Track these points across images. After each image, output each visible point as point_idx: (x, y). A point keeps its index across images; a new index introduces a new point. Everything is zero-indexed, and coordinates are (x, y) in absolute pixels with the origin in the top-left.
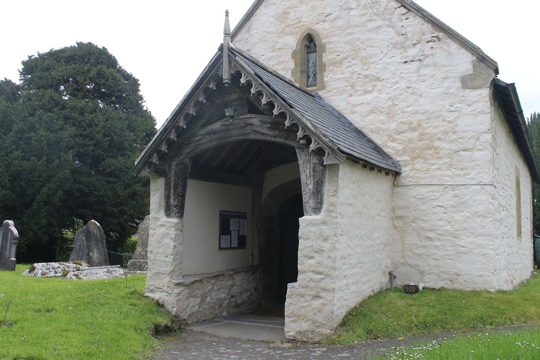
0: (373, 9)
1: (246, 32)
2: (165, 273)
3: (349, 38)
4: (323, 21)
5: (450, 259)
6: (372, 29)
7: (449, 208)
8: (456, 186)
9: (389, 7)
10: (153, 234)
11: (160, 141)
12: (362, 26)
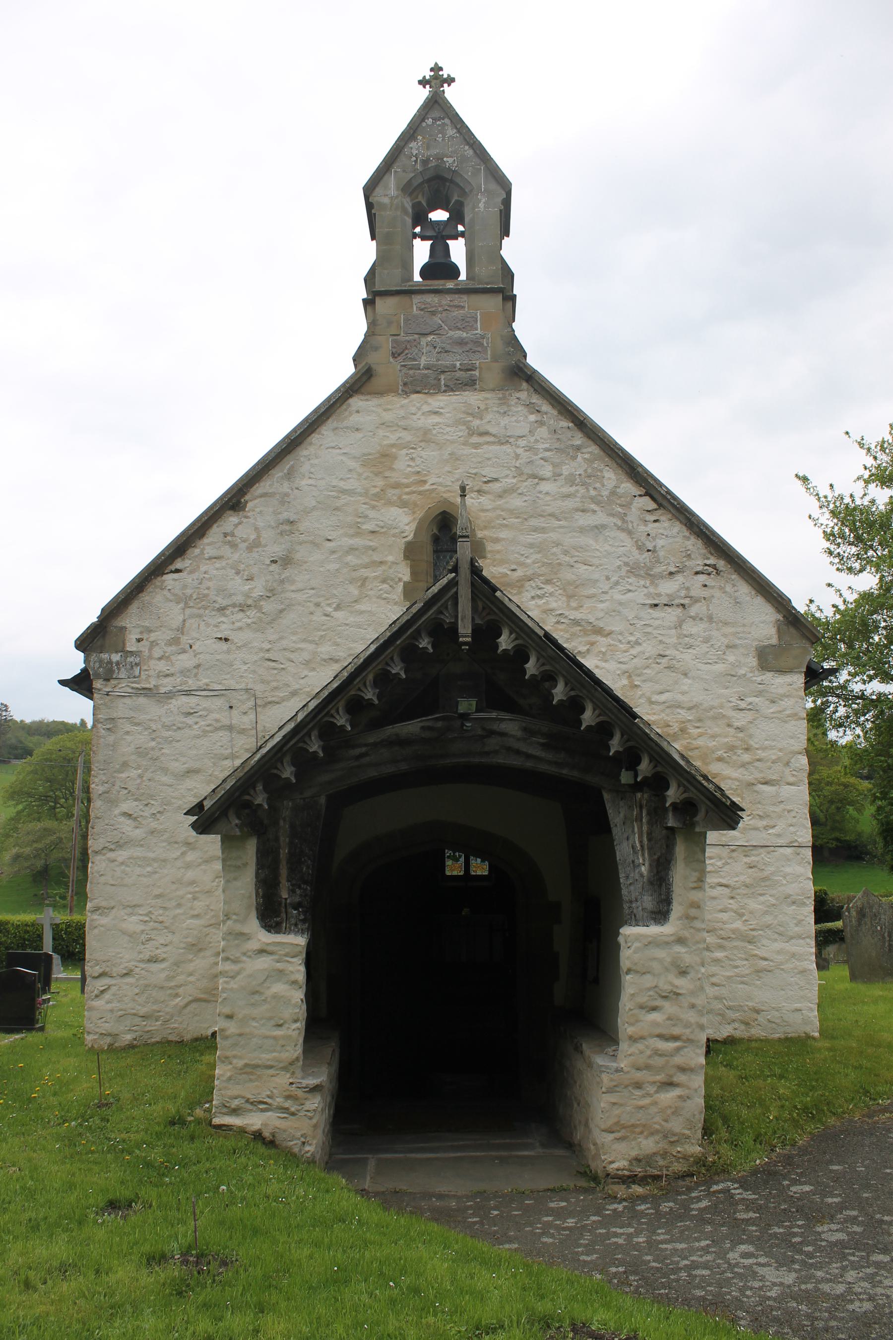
0: (587, 489)
1: (282, 478)
2: (276, 1064)
3: (538, 537)
4: (479, 491)
5: (743, 983)
6: (587, 528)
7: (739, 888)
8: (751, 848)
9: (620, 491)
10: (232, 974)
11: (279, 755)
12: (566, 518)
